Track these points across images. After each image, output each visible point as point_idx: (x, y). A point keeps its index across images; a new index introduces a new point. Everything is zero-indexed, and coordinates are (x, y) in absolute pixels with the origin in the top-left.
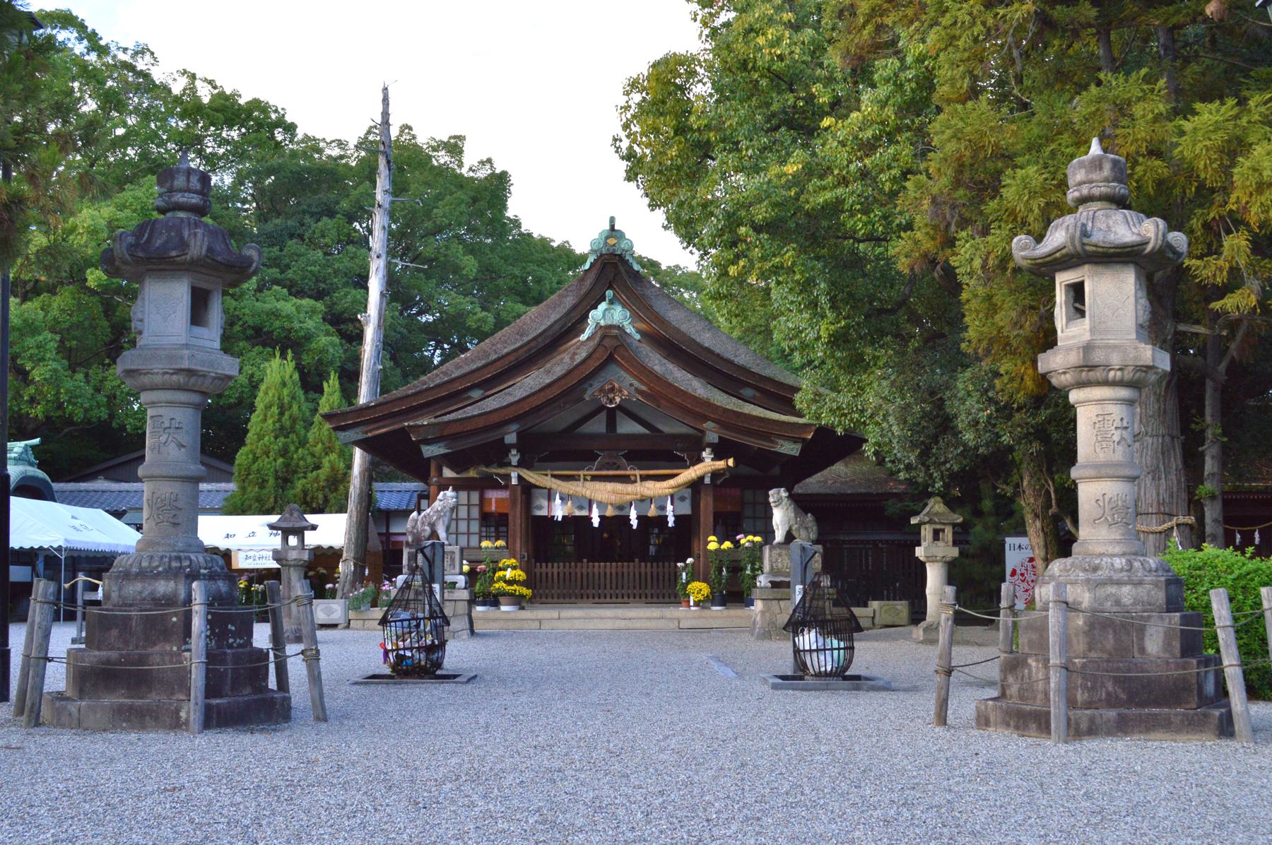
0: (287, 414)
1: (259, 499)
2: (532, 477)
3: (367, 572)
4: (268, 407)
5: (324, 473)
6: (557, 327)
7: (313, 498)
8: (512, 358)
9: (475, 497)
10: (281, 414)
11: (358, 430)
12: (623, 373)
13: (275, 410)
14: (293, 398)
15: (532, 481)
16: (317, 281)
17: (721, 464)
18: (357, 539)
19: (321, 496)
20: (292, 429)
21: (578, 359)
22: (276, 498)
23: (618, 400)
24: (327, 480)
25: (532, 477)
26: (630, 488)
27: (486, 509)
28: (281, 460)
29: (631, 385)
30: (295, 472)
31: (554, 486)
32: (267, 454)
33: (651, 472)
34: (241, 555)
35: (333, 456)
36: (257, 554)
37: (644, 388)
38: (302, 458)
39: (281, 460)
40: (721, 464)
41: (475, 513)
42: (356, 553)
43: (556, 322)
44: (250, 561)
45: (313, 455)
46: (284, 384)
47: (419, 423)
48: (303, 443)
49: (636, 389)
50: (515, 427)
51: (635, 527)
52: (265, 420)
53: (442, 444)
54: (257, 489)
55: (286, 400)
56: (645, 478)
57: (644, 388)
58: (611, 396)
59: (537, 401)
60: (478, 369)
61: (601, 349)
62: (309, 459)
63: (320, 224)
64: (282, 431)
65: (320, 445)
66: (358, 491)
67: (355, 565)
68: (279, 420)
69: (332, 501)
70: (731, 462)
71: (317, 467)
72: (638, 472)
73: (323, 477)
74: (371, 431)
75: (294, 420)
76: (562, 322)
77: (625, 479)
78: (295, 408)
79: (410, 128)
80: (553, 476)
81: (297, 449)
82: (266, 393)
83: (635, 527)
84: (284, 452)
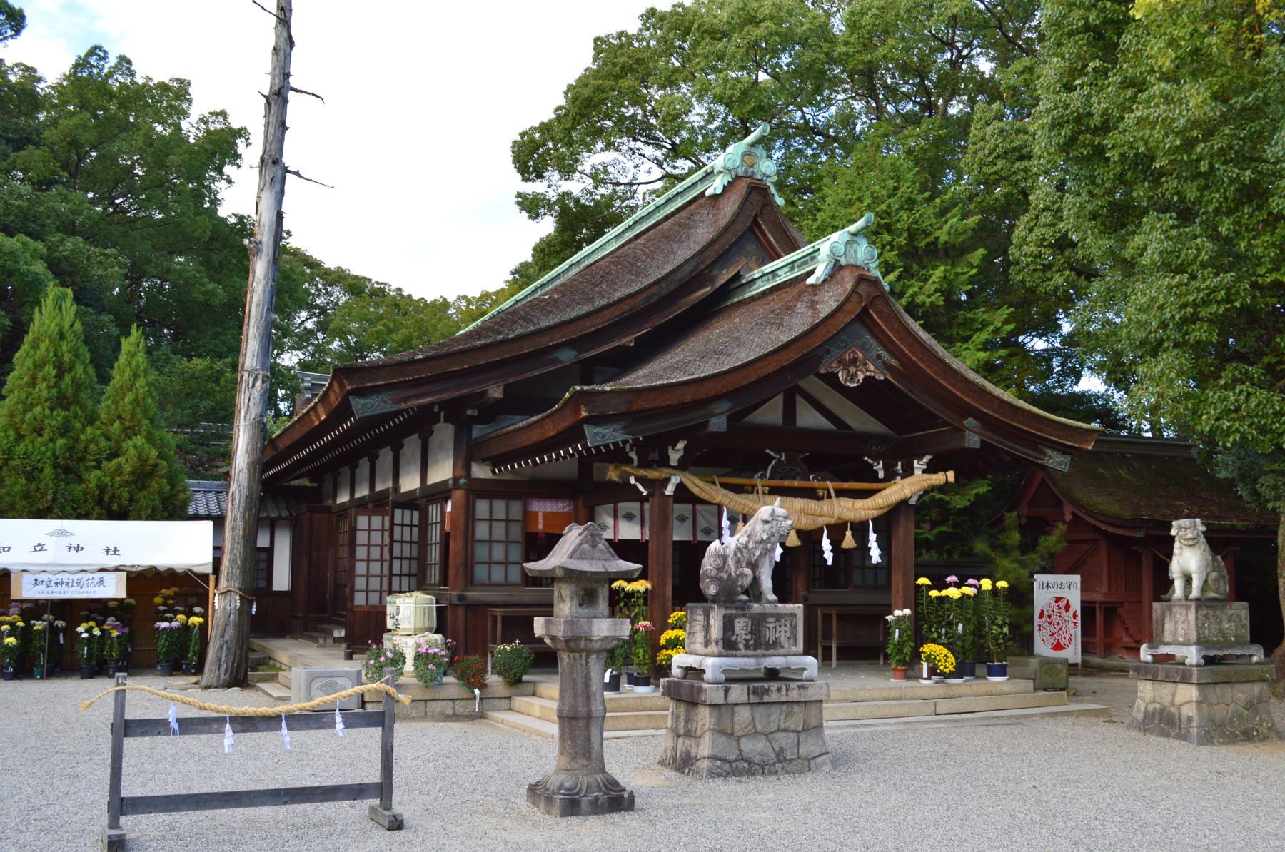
0: (67, 378)
1: (26, 496)
2: (696, 485)
3: (254, 610)
4: (39, 366)
5: (127, 463)
6: (687, 269)
7: (112, 497)
8: (626, 307)
9: (516, 508)
10: (59, 376)
11: (385, 396)
12: (869, 338)
13: (50, 370)
14: (77, 356)
15: (696, 491)
16: (26, 218)
17: (938, 478)
18: (244, 561)
19: (126, 495)
20: (76, 400)
21: (825, 310)
22: (55, 493)
23: (861, 377)
24: (132, 473)
25: (696, 485)
26: (824, 506)
27: (532, 529)
28: (61, 442)
29: (879, 357)
30: (82, 459)
31: (725, 501)
32: (39, 431)
33: (786, 483)
34: (27, 579)
35: (139, 440)
36: (54, 578)
37: (894, 362)
38: (93, 440)
39: (61, 442)
40: (938, 478)
41: (516, 533)
42: (243, 582)
43: (687, 261)
44: (43, 587)
45: (108, 439)
46: (62, 336)
47: (598, 388)
48: (91, 420)
49: (884, 363)
50: (724, 406)
51: (829, 563)
52: (33, 383)
53: (617, 426)
54: (23, 481)
55: (67, 357)
56: (840, 493)
57: (894, 362)
58: (852, 370)
59: (769, 368)
60: (579, 318)
61: (855, 298)
62: (103, 443)
63: (22, 153)
64: (62, 402)
65: (117, 424)
66: (245, 492)
67: (242, 598)
68: (56, 385)
69: (142, 502)
70: (951, 476)
71: (114, 455)
72: (830, 484)
73: (127, 468)
74: (406, 400)
75: (78, 386)
76: (694, 263)
77: (811, 494)
78: (79, 369)
79: (129, 62)
80: (724, 486)
81: (84, 427)
82: (35, 347)
83: (829, 563)
84: (65, 430)
